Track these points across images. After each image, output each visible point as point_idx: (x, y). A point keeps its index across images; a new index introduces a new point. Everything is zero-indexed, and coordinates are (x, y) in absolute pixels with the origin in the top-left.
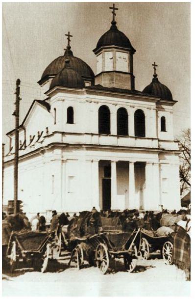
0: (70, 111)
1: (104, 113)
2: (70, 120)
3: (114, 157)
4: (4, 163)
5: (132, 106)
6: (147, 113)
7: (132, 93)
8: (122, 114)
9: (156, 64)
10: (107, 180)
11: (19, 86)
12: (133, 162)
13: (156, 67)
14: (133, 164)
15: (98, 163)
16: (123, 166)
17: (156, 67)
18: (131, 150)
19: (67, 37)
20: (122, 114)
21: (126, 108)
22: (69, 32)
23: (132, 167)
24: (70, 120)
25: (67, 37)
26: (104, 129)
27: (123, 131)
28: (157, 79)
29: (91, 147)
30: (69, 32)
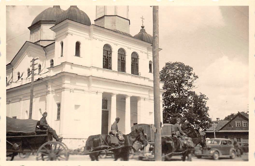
0: (78, 45)
1: (107, 50)
2: (78, 53)
3: (116, 91)
4: (9, 92)
5: (130, 49)
6: (140, 54)
7: (126, 36)
8: (122, 53)
9: (144, 18)
10: (8, 136)
11: (155, 50)
12: (130, 96)
13: (143, 20)
14: (130, 97)
15: (102, 94)
16: (121, 99)
17: (143, 20)
18: (20, 89)
19: (142, 19)
20: (122, 53)
21: (136, 52)
22: (143, 16)
23: (128, 101)
24: (78, 53)
25: (142, 19)
26: (107, 64)
27: (122, 67)
28: (145, 30)
29: (98, 80)
30: (143, 16)
